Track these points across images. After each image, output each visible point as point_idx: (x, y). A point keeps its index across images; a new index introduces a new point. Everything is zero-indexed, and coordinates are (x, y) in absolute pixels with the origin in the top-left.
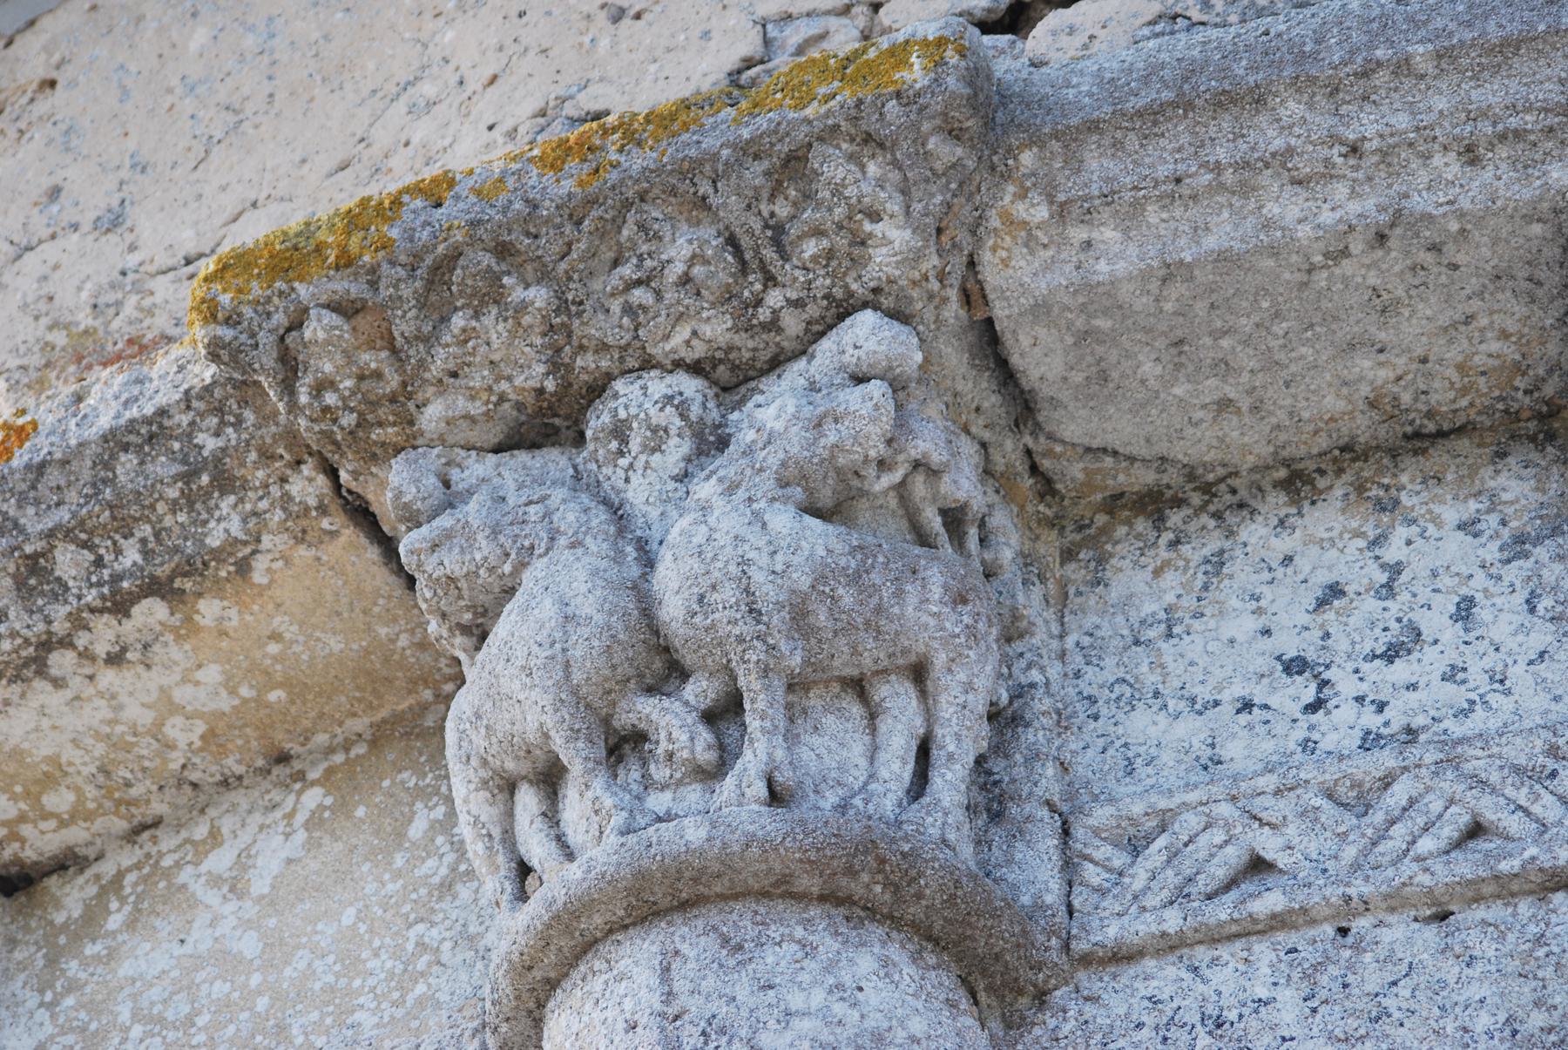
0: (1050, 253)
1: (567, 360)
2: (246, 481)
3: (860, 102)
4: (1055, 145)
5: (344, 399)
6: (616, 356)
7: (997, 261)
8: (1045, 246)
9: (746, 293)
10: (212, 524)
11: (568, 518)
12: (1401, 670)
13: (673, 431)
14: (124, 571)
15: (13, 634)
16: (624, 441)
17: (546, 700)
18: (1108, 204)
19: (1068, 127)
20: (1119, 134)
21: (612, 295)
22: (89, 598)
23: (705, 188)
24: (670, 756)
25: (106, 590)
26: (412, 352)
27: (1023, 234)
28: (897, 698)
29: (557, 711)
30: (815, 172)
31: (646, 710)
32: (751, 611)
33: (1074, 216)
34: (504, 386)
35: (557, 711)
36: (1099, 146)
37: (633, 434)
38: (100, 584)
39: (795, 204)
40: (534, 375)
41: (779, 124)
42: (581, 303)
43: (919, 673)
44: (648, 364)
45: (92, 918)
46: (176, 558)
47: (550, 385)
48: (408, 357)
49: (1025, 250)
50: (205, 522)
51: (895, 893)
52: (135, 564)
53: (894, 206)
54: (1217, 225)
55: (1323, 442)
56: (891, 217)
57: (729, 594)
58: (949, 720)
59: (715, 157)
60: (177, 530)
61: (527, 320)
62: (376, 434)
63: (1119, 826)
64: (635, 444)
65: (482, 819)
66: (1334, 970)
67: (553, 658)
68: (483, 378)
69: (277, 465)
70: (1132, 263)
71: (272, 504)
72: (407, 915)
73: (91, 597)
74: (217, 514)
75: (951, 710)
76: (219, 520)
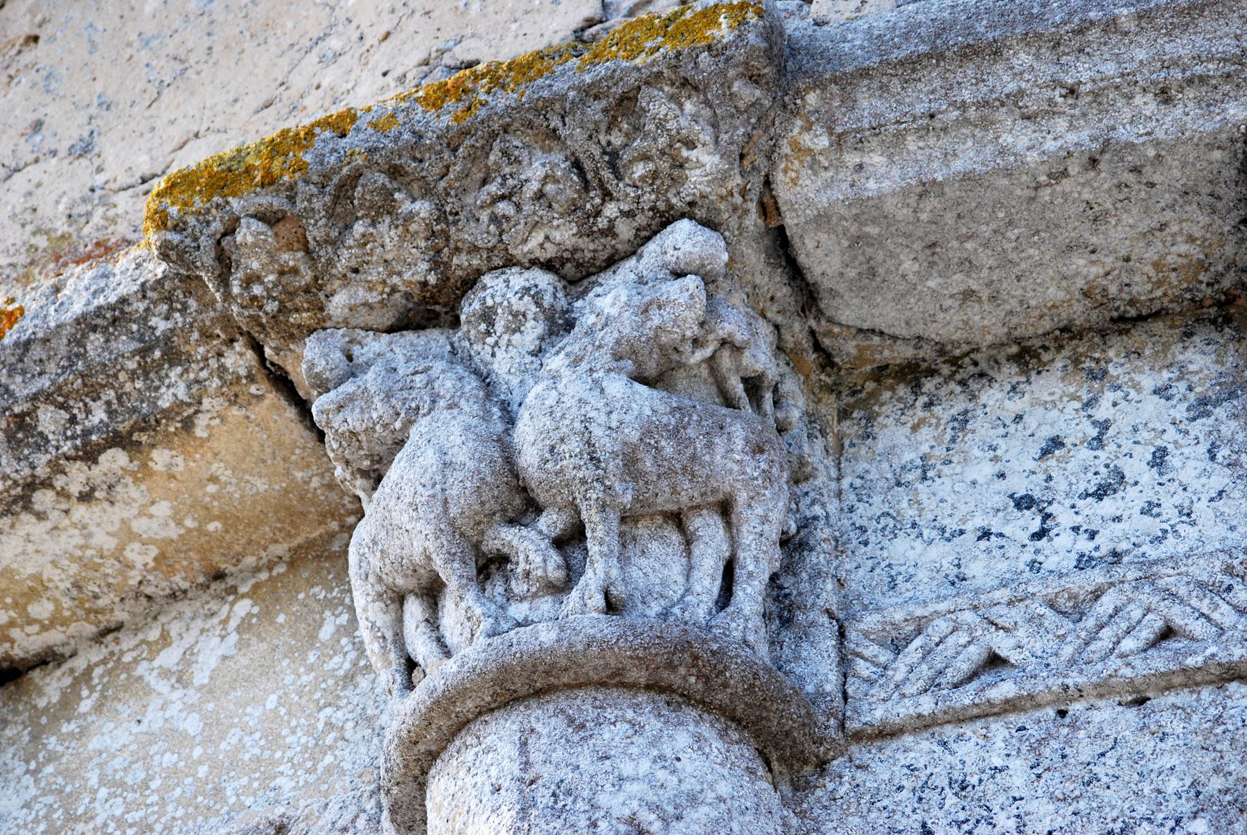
1: (445, 259)
2: (190, 355)
3: (679, 54)
4: (834, 88)
5: (268, 290)
6: (485, 256)
7: (788, 180)
8: (826, 168)
9: (588, 206)
10: (163, 390)
11: (446, 385)
12: (1108, 506)
13: (530, 316)
14: (93, 427)
16: (491, 323)
17: (429, 530)
18: (876, 135)
19: (845, 74)
20: (885, 79)
21: (482, 207)
23: (555, 122)
24: (527, 574)
25: (78, 442)
26: (321, 253)
27: (809, 158)
28: (709, 528)
30: (643, 109)
32: (592, 459)
36: (869, 89)
37: (498, 318)
38: (73, 437)
39: (627, 135)
40: (419, 271)
41: (614, 71)
42: (457, 214)
43: (725, 509)
44: (510, 262)
45: (67, 703)
46: (135, 417)
47: (432, 279)
48: (319, 257)
51: (706, 683)
52: (101, 421)
53: (706, 137)
54: (963, 152)
55: (1047, 325)
56: (704, 145)
57: (574, 445)
58: (749, 545)
59: (564, 97)
60: (135, 394)
61: (413, 227)
62: (294, 318)
63: (884, 630)
64: (499, 326)
65: (378, 624)
66: (1054, 744)
67: (434, 496)
69: (215, 342)
70: (895, 182)
71: (211, 374)
72: (318, 701)
73: (67, 447)
74: (167, 381)
76: (168, 387)
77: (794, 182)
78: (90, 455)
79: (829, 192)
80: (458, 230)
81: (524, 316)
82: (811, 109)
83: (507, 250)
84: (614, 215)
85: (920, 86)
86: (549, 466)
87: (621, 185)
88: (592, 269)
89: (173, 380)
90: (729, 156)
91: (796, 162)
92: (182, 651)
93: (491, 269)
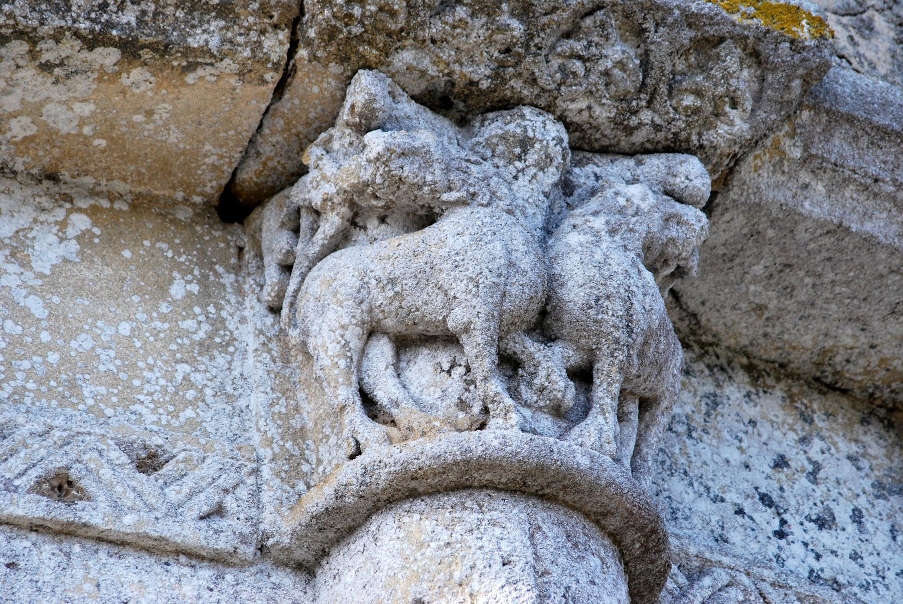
0: (783, 178)
1: (507, 77)
2: (238, 18)
3: (768, 31)
4: (824, 118)
5: (363, 15)
6: (536, 93)
7: (753, 165)
8: (783, 172)
9: (634, 103)
10: (199, 31)
13: (555, 163)
14: (118, 24)
15: (11, 15)
16: (525, 151)
17: (484, 310)
18: (834, 171)
19: (838, 112)
20: (860, 133)
21: (559, 55)
22: (82, 26)
23: (649, 25)
24: (542, 389)
25: (98, 28)
26: (422, 14)
27: (778, 158)
29: (488, 320)
30: (718, 56)
31: (531, 348)
32: (628, 326)
33: (812, 166)
34: (456, 67)
35: (488, 320)
36: (845, 133)
37: (532, 151)
38: (93, 21)
39: (690, 66)
41: (716, 14)
42: (540, 48)
44: (548, 109)
46: (160, 38)
47: (485, 85)
48: (418, 15)
49: (771, 168)
50: (193, 26)
51: (643, 553)
52: (128, 23)
53: (749, 105)
54: (877, 218)
55: (774, 355)
56: (744, 111)
57: (617, 306)
58: (653, 445)
59: (670, 11)
60: (171, 19)
61: (499, 37)
62: (363, 49)
63: (678, 555)
64: (532, 157)
65: (351, 345)
67: (498, 285)
68: (450, 55)
69: (266, 20)
70: (823, 213)
71: (246, 43)
72: (174, 353)
73: (83, 25)
74: (206, 26)
75: (655, 439)
76: (204, 31)
77: (757, 169)
78: (91, 42)
79: (776, 192)
80: (534, 62)
81: (551, 161)
82: (800, 122)
83: (556, 98)
84: (647, 121)
85: (879, 152)
86: (592, 312)
87: (668, 103)
88: (586, 146)
89: (212, 28)
90: (756, 131)
91: (768, 155)
92: (14, 229)
93: (532, 105)
